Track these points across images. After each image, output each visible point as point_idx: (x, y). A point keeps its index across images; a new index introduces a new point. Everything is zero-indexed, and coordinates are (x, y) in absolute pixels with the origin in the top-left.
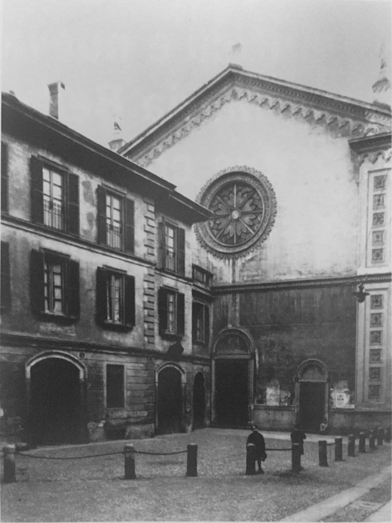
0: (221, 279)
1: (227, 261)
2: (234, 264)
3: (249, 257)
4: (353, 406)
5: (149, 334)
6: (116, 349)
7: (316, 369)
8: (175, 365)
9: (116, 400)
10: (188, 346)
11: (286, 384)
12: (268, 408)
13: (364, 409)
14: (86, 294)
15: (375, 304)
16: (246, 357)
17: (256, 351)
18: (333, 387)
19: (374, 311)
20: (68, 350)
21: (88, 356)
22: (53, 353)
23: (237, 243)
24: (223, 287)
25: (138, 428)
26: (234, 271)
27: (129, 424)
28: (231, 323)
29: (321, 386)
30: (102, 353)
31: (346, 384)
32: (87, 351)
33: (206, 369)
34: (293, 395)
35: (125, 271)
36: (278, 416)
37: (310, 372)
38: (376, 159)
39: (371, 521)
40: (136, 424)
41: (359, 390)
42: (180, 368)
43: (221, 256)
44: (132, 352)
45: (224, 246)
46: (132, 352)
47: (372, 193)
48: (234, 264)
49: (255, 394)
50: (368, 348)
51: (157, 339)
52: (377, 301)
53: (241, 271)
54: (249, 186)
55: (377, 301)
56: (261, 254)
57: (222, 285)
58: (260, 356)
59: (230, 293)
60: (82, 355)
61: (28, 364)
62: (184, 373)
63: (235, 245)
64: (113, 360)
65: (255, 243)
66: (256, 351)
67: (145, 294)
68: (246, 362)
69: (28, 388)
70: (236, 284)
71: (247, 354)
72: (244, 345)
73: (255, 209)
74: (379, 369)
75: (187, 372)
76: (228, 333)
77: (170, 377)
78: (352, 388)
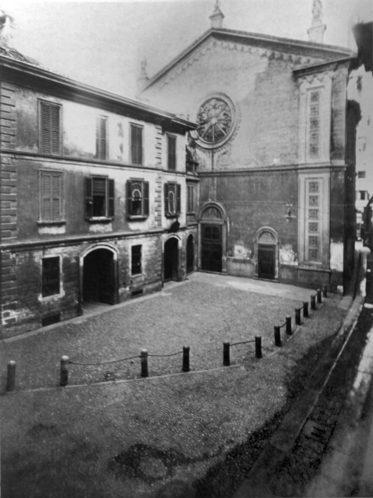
0: (204, 166)
1: (208, 154)
2: (213, 156)
3: (222, 151)
4: (296, 264)
5: (158, 220)
6: (137, 235)
7: (269, 235)
8: (174, 235)
9: (137, 269)
10: (182, 220)
11: (249, 244)
12: (235, 261)
13: (305, 267)
14: (119, 198)
15: (312, 189)
16: (221, 223)
17: (228, 219)
18: (281, 248)
19: (312, 194)
20: (107, 241)
21: (120, 242)
22: (97, 245)
23: (215, 141)
24: (205, 173)
25: (150, 287)
26: (213, 161)
27: (144, 284)
28: (211, 198)
29: (273, 246)
30: (128, 239)
31: (291, 247)
32: (119, 239)
33: (195, 230)
34: (253, 253)
35: (143, 179)
36: (243, 266)
37: (264, 235)
38: (313, 80)
39: (306, 497)
40: (149, 284)
41: (301, 253)
42: (177, 236)
43: (204, 150)
44: (147, 234)
45: (206, 143)
46: (147, 234)
47: (308, 194)
48: (213, 156)
49: (227, 250)
50: (307, 234)
51: (163, 218)
52: (314, 187)
53: (218, 161)
54: (223, 101)
55: (314, 187)
56: (230, 149)
57: (205, 171)
58: (230, 223)
59: (210, 177)
60: (116, 243)
61: (82, 256)
62: (180, 239)
63: (214, 142)
64: (135, 242)
65: (227, 142)
66: (228, 219)
67: (156, 201)
68: (221, 226)
69: (81, 273)
70: (214, 171)
71: (222, 221)
72: (219, 213)
73: (227, 118)
74: (316, 237)
75: (181, 237)
76: (209, 206)
77: (172, 244)
78: (295, 249)
